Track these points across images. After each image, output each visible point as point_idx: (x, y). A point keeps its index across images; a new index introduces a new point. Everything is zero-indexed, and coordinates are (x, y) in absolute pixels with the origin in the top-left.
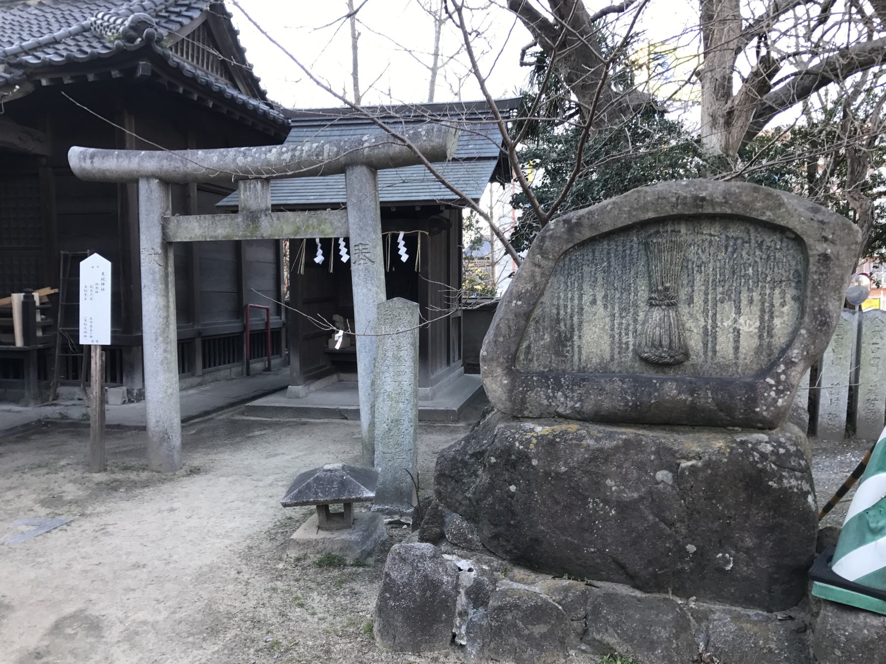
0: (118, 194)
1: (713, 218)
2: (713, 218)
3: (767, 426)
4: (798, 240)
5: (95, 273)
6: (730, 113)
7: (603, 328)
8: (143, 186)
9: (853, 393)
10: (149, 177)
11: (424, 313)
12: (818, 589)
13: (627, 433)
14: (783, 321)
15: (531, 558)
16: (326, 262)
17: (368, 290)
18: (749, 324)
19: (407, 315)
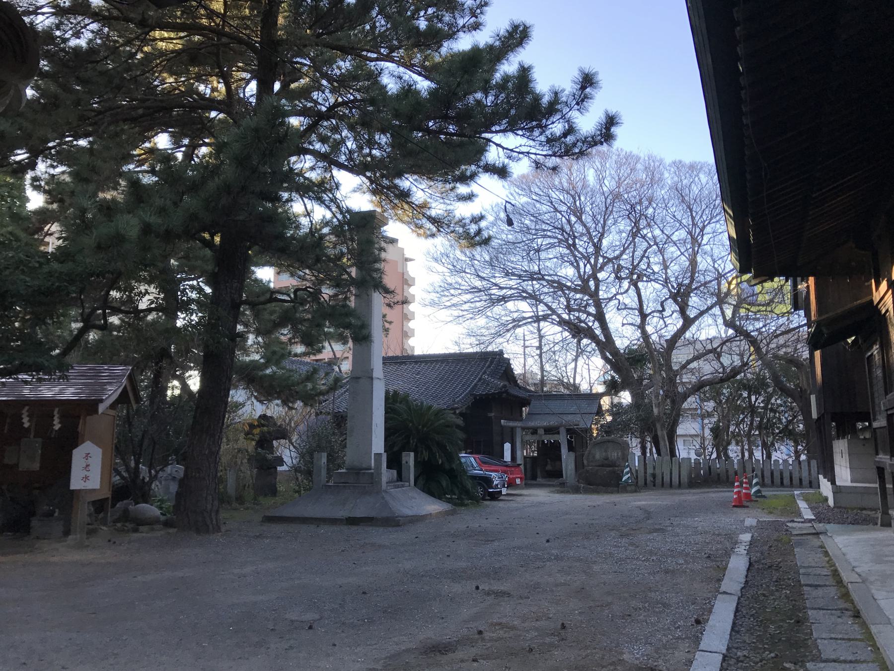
0: (513, 429)
5: (507, 446)
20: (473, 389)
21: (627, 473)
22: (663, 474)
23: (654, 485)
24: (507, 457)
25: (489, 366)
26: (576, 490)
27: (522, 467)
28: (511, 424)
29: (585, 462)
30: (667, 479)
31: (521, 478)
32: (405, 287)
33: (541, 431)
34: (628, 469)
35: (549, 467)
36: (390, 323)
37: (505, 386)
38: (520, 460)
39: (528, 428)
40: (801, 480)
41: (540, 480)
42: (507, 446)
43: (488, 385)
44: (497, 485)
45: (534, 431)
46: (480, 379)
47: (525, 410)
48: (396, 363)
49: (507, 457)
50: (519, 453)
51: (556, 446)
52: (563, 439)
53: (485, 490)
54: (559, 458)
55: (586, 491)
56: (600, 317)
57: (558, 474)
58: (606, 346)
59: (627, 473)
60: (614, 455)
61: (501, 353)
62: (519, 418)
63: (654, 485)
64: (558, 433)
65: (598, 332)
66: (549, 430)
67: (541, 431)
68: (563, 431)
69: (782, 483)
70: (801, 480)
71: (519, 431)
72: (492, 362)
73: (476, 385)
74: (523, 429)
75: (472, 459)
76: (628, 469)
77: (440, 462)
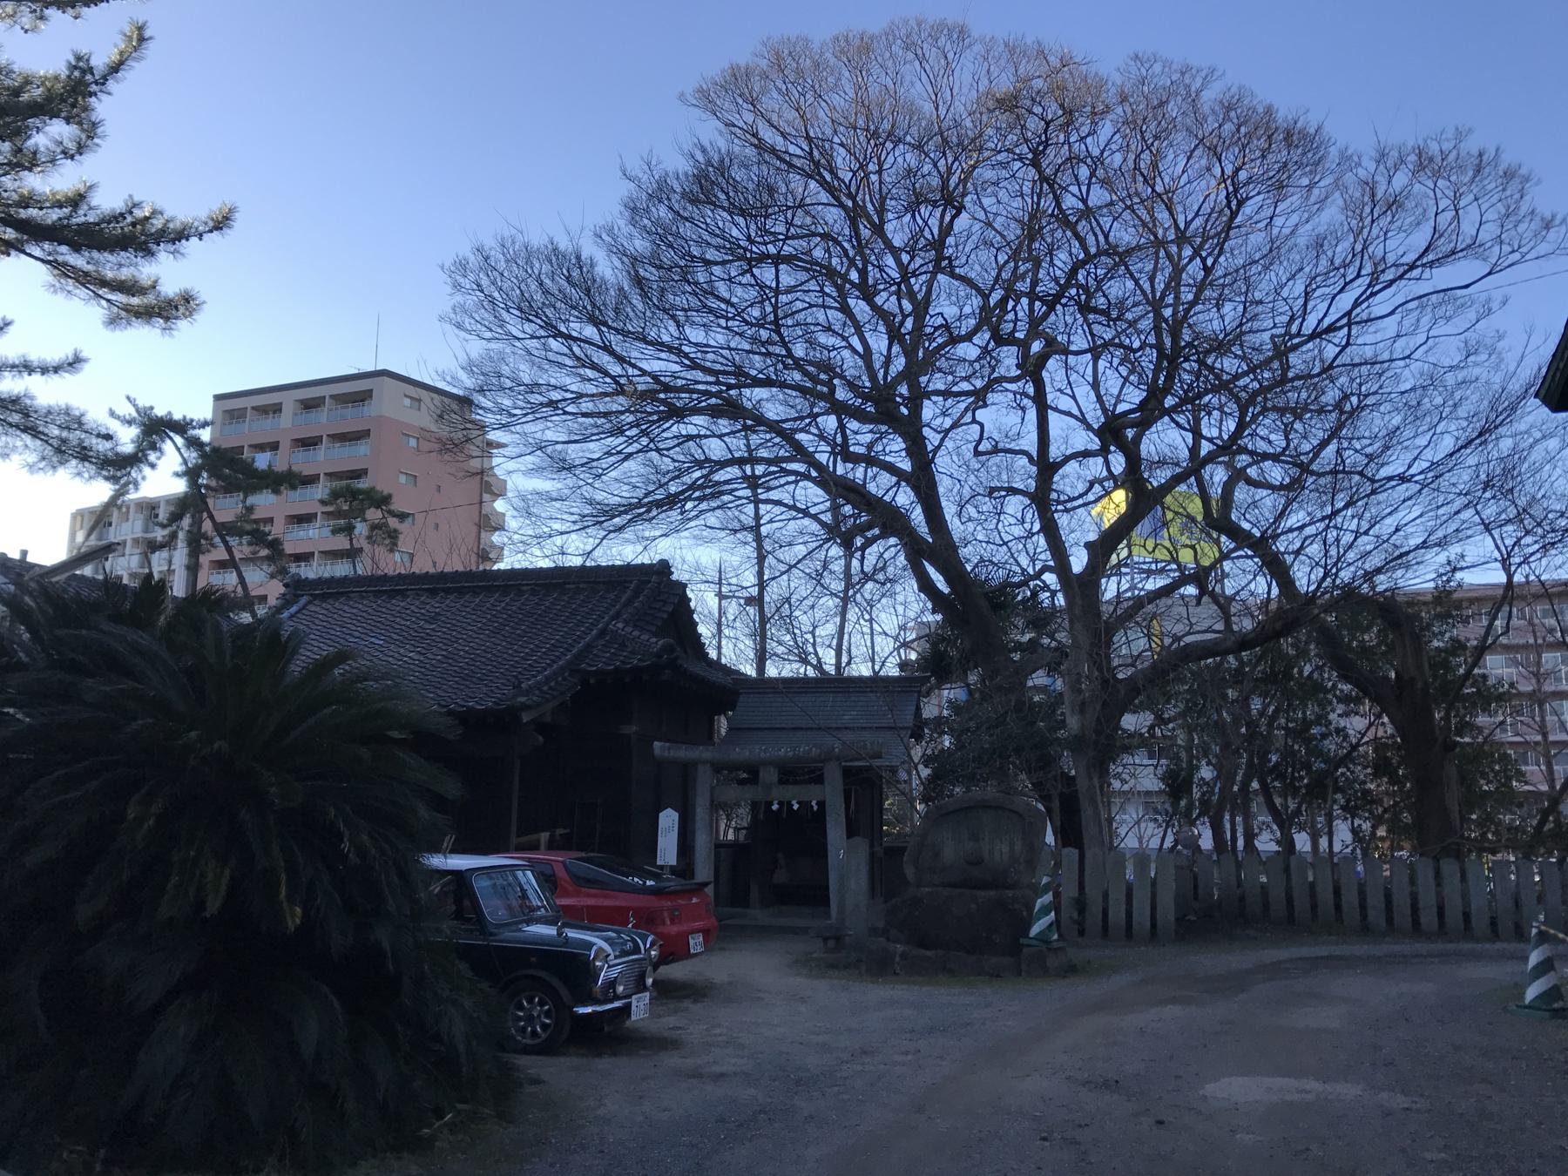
0: (687, 771)
1: (990, 807)
2: (990, 807)
3: (1010, 887)
4: (1021, 816)
5: (668, 820)
6: (1083, 704)
7: (952, 849)
8: (701, 768)
9: (1153, 908)
10: (705, 762)
11: (872, 846)
12: (1023, 941)
13: (959, 891)
14: (1018, 847)
15: (923, 945)
16: (779, 810)
17: (835, 832)
18: (1005, 849)
19: (862, 846)
20: (579, 657)
21: (1045, 911)
22: (1106, 896)
23: (1081, 933)
24: (667, 850)
25: (630, 602)
26: (880, 967)
27: (710, 890)
28: (683, 753)
29: (909, 872)
30: (1117, 914)
31: (706, 933)
32: (486, 497)
33: (769, 775)
34: (1048, 898)
35: (781, 877)
36: (402, 517)
37: (668, 649)
38: (703, 871)
39: (733, 767)
40: (1467, 916)
41: (758, 915)
42: (668, 820)
43: (623, 646)
44: (612, 984)
45: (752, 773)
46: (603, 633)
47: (723, 724)
48: (378, 594)
49: (667, 850)
50: (702, 842)
51: (816, 820)
52: (831, 792)
53: (561, 1009)
54: (819, 851)
55: (915, 970)
56: (923, 480)
57: (815, 895)
58: (932, 550)
59: (1045, 911)
60: (1000, 849)
61: (664, 568)
62: (709, 735)
63: (1081, 933)
64: (819, 779)
65: (918, 516)
66: (791, 773)
67: (769, 775)
68: (833, 776)
69: (1416, 923)
70: (1467, 916)
71: (704, 781)
72: (637, 593)
73: (589, 646)
74: (718, 768)
75: (529, 879)
76: (1048, 898)
77: (294, 917)
